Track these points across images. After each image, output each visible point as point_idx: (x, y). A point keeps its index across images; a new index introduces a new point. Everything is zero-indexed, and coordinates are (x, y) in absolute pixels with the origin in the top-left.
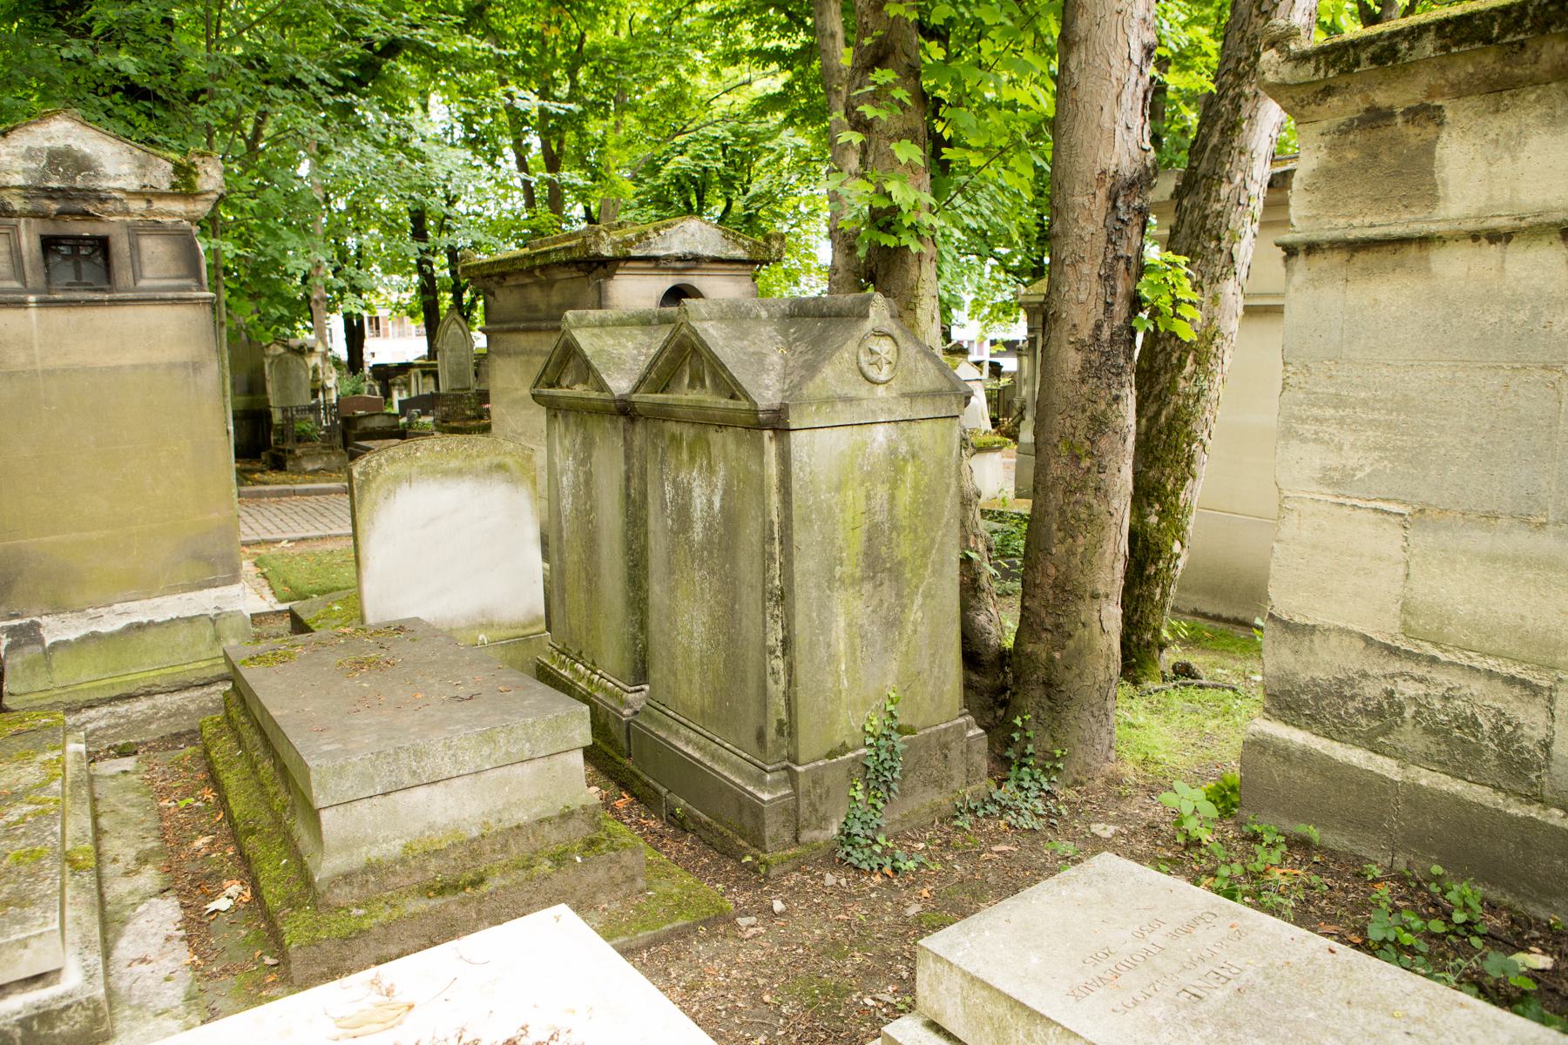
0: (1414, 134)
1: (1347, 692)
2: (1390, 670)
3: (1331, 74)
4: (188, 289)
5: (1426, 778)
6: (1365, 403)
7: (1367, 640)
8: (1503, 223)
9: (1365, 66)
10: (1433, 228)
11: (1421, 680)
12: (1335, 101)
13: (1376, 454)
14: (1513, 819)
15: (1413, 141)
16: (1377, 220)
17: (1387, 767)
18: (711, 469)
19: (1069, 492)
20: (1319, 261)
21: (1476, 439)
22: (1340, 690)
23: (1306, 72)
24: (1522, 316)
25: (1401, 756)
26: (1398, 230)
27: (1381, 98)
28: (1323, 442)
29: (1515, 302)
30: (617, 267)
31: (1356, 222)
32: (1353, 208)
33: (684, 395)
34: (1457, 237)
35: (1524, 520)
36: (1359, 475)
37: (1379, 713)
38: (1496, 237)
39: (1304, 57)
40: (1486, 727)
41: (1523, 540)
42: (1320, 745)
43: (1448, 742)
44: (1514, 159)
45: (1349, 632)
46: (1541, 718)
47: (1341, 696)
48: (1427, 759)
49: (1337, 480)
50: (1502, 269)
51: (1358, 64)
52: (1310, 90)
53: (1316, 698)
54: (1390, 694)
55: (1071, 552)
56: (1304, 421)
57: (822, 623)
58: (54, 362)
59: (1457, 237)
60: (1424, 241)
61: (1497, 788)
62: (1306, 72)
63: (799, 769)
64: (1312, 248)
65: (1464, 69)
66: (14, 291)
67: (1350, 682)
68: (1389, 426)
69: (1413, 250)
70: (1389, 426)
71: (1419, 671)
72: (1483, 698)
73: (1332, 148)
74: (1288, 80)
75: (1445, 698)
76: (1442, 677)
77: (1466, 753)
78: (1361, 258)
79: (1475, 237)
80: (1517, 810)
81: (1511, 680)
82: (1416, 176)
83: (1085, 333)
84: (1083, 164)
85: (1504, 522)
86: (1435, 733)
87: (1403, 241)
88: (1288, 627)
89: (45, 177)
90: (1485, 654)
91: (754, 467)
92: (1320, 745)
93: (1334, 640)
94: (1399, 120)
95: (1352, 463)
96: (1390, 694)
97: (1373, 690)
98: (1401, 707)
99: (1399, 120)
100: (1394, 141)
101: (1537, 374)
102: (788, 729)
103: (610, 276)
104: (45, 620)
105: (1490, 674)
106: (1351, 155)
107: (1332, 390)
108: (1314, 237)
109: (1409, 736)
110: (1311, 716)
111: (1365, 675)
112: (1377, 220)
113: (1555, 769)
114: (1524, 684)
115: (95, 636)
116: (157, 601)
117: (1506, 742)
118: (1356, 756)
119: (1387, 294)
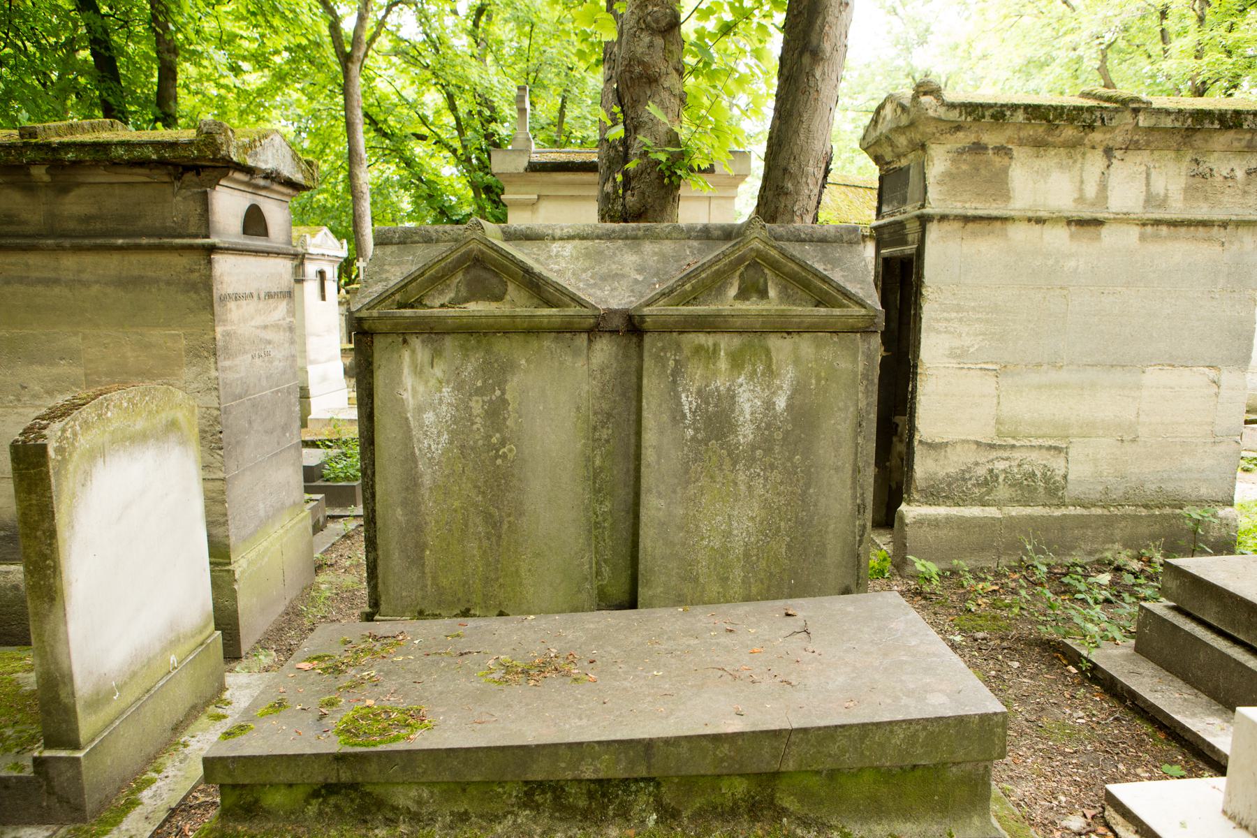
0: (998, 161)
1: (967, 476)
2: (991, 457)
3: (969, 119)
5: (1016, 511)
6: (974, 309)
7: (978, 444)
9: (988, 119)
10: (1012, 213)
11: (1007, 459)
12: (961, 135)
13: (981, 337)
14: (1057, 518)
15: (998, 165)
16: (979, 205)
17: (992, 512)
18: (770, 372)
20: (946, 226)
21: (1031, 326)
22: (963, 477)
23: (954, 115)
24: (1050, 262)
25: (997, 504)
26: (995, 213)
28: (950, 333)
30: (225, 176)
31: (967, 205)
32: (966, 197)
35: (1053, 365)
36: (972, 350)
37: (986, 483)
38: (1040, 221)
39: (952, 106)
40: (1039, 474)
42: (955, 511)
43: (1022, 488)
44: (1046, 183)
45: (967, 441)
46: (1062, 462)
47: (964, 480)
49: (958, 355)
50: (1041, 238)
51: (983, 117)
52: (949, 125)
53: (949, 485)
54: (991, 471)
56: (938, 321)
60: (1004, 219)
61: (1044, 505)
62: (954, 115)
63: (80, 754)
65: (1029, 132)
67: (969, 470)
68: (987, 321)
69: (998, 224)
70: (987, 321)
71: (1005, 455)
72: (1037, 460)
73: (953, 161)
74: (943, 117)
75: (1019, 466)
76: (1017, 455)
77: (1030, 492)
78: (970, 226)
79: (1030, 220)
80: (1058, 513)
81: (1050, 448)
82: (998, 185)
85: (1045, 367)
86: (1014, 485)
87: (996, 219)
88: (932, 446)
90: (1037, 438)
93: (959, 448)
94: (990, 152)
95: (967, 343)
96: (991, 471)
97: (982, 471)
98: (997, 477)
99: (990, 152)
100: (988, 163)
101: (1058, 291)
103: (214, 183)
105: (1041, 447)
106: (964, 167)
107: (955, 302)
108: (947, 212)
109: (1003, 492)
110: (947, 497)
111: (977, 464)
112: (979, 205)
113: (1070, 487)
114: (1056, 448)
117: (1047, 479)
118: (975, 511)
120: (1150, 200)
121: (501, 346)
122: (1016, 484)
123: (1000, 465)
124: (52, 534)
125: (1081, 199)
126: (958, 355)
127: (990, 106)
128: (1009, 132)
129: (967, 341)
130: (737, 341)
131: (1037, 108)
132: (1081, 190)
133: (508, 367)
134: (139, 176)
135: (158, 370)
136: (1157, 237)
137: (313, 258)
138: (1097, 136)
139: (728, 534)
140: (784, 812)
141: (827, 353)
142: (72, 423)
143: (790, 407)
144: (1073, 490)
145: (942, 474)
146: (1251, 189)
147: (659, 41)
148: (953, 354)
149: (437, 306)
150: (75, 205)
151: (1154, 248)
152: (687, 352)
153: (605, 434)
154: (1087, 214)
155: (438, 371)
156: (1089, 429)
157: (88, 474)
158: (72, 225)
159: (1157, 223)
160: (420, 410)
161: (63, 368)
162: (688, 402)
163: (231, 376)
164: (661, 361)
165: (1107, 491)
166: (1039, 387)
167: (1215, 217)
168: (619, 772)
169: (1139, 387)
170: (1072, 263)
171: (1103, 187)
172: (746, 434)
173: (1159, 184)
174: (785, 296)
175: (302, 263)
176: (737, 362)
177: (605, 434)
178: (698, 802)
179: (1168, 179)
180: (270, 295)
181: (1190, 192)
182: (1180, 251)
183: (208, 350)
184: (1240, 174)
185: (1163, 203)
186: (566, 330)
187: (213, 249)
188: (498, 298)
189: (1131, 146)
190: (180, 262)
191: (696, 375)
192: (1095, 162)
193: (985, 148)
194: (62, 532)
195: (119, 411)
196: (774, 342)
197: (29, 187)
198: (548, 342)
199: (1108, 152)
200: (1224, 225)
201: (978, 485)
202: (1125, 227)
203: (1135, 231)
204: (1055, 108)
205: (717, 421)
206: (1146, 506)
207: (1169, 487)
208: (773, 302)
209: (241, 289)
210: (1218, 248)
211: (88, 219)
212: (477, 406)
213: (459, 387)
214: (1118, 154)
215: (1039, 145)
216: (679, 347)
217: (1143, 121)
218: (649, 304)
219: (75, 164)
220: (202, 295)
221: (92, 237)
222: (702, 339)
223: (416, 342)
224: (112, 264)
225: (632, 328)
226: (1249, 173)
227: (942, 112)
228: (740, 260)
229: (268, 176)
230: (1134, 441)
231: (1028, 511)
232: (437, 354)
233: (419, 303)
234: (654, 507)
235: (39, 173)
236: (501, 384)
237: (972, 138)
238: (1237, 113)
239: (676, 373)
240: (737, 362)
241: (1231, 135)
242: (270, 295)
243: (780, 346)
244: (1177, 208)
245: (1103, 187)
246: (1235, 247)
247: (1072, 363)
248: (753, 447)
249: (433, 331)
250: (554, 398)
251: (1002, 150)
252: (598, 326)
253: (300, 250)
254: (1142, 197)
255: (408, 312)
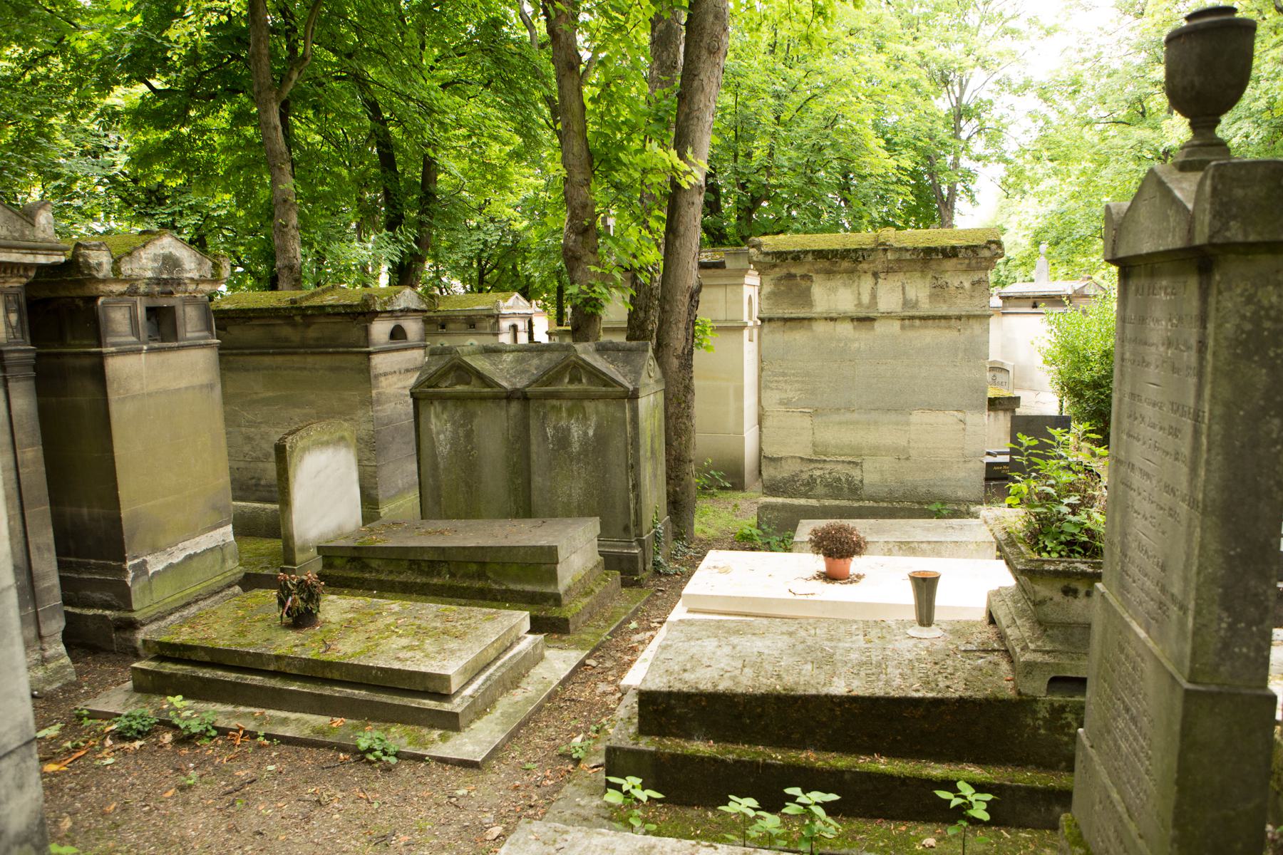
0: (803, 283)
4: (206, 338)
7: (802, 459)
8: (834, 315)
18: (586, 418)
19: (677, 418)
20: (773, 325)
22: (793, 479)
26: (801, 315)
27: (793, 271)
29: (839, 340)
33: (565, 385)
34: (820, 319)
35: (848, 409)
37: (808, 484)
38: (832, 319)
39: (767, 254)
41: (849, 416)
42: (789, 501)
48: (826, 496)
49: (785, 403)
55: (680, 444)
57: (1123, 346)
58: (152, 388)
59: (820, 319)
60: (810, 319)
62: (768, 259)
64: (770, 320)
66: (134, 343)
67: (797, 475)
69: (806, 322)
70: (803, 382)
76: (828, 466)
78: (792, 324)
80: (856, 505)
81: (850, 462)
82: (805, 297)
83: (680, 352)
84: (681, 284)
87: (804, 319)
89: (161, 273)
91: (618, 415)
92: (789, 501)
97: (805, 476)
100: (797, 285)
102: (638, 523)
103: (371, 321)
104: (148, 558)
109: (820, 490)
115: (171, 566)
116: (197, 539)
117: (849, 483)
118: (802, 501)
119: (798, 337)
120: (906, 303)
121: (470, 405)
122: (828, 485)
123: (818, 473)
124: (287, 479)
125: (859, 304)
126: (785, 403)
127: (791, 252)
128: (807, 267)
129: (790, 395)
130: (570, 403)
131: (821, 251)
132: (859, 299)
133: (473, 415)
134: (338, 319)
135: (344, 413)
136: (912, 327)
137: (505, 317)
138: (865, 266)
139: (570, 495)
140: (489, 578)
141: (611, 409)
142: (297, 437)
143: (595, 435)
144: (868, 490)
145: (779, 477)
146: (976, 294)
147: (580, 238)
148: (781, 403)
149: (444, 388)
150: (312, 333)
151: (911, 334)
152: (548, 408)
153: (517, 446)
154: (863, 315)
155: (445, 416)
156: (875, 451)
157: (302, 457)
158: (311, 342)
159: (912, 318)
160: (438, 434)
161: (307, 410)
162: (550, 432)
163: (381, 414)
164: (537, 412)
165: (891, 492)
166: (840, 423)
167: (950, 313)
168: (435, 558)
169: (908, 424)
170: (856, 345)
171: (874, 296)
172: (576, 447)
173: (912, 293)
174: (590, 382)
175: (497, 321)
176: (570, 414)
177: (517, 446)
178: (462, 572)
179: (919, 290)
180: (407, 371)
181: (933, 297)
182: (928, 336)
183: (369, 402)
184: (967, 285)
185: (915, 305)
186: (496, 398)
187: (370, 353)
188: (468, 384)
189: (889, 271)
190: (356, 359)
191: (552, 418)
192: (867, 283)
193: (794, 276)
194: (291, 479)
195: (315, 432)
196: (586, 403)
197: (294, 325)
198: (489, 404)
199: (875, 275)
200: (959, 318)
201: (802, 485)
202: (890, 322)
203: (897, 324)
204: (832, 251)
205: (563, 440)
206: (919, 503)
207: (936, 490)
208: (584, 385)
209: (388, 370)
210: (956, 333)
211: (317, 339)
212: (461, 432)
213: (454, 424)
214: (882, 275)
215: (829, 273)
216: (545, 406)
217: (890, 256)
218: (528, 386)
219: (312, 315)
220: (365, 375)
221: (319, 348)
222: (555, 402)
223: (436, 403)
224: (327, 361)
225: (521, 397)
226: (973, 284)
227: (761, 257)
228: (568, 366)
229: (401, 311)
230: (907, 459)
231: (837, 502)
232: (444, 408)
233: (436, 386)
234: (537, 481)
235: (298, 319)
236: (471, 422)
237: (784, 271)
238: (954, 248)
239: (544, 417)
240: (570, 414)
241: (954, 261)
242: (407, 371)
243: (590, 406)
244: (926, 308)
245: (874, 296)
246: (968, 332)
247: (861, 408)
248: (579, 453)
249: (443, 398)
250: (493, 430)
251: (806, 277)
252: (510, 396)
253: (496, 312)
254: (901, 302)
255: (431, 390)
